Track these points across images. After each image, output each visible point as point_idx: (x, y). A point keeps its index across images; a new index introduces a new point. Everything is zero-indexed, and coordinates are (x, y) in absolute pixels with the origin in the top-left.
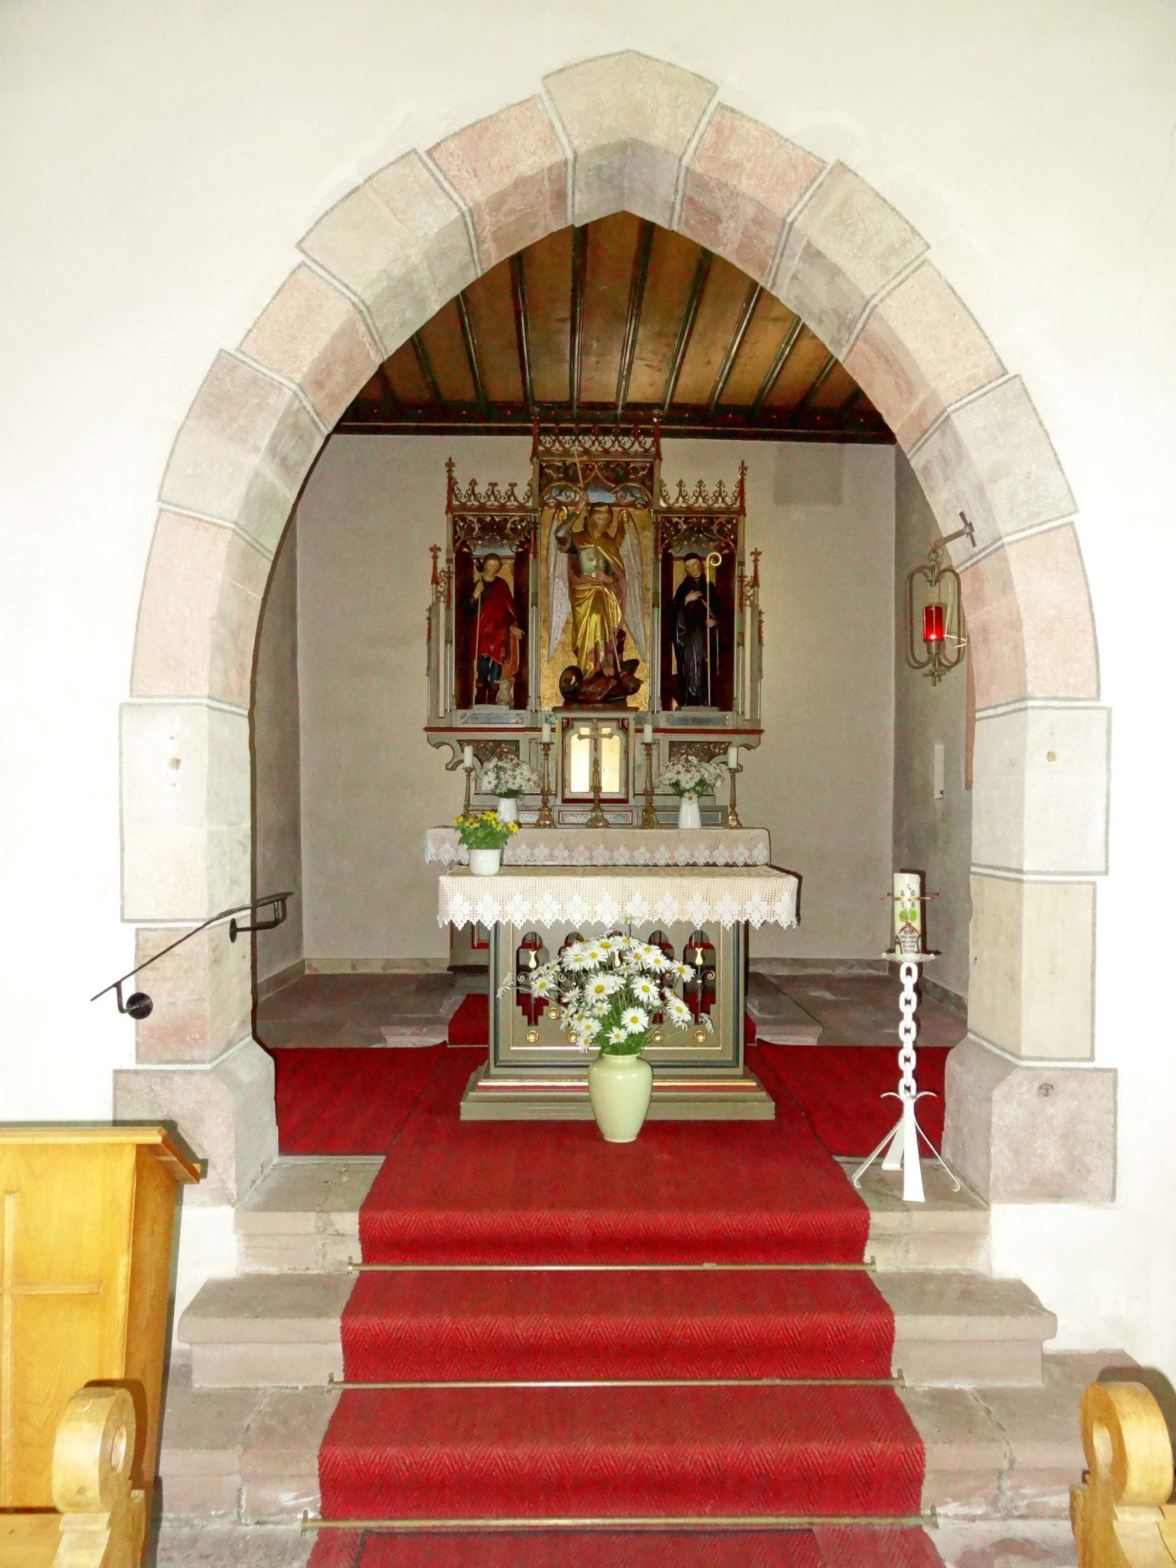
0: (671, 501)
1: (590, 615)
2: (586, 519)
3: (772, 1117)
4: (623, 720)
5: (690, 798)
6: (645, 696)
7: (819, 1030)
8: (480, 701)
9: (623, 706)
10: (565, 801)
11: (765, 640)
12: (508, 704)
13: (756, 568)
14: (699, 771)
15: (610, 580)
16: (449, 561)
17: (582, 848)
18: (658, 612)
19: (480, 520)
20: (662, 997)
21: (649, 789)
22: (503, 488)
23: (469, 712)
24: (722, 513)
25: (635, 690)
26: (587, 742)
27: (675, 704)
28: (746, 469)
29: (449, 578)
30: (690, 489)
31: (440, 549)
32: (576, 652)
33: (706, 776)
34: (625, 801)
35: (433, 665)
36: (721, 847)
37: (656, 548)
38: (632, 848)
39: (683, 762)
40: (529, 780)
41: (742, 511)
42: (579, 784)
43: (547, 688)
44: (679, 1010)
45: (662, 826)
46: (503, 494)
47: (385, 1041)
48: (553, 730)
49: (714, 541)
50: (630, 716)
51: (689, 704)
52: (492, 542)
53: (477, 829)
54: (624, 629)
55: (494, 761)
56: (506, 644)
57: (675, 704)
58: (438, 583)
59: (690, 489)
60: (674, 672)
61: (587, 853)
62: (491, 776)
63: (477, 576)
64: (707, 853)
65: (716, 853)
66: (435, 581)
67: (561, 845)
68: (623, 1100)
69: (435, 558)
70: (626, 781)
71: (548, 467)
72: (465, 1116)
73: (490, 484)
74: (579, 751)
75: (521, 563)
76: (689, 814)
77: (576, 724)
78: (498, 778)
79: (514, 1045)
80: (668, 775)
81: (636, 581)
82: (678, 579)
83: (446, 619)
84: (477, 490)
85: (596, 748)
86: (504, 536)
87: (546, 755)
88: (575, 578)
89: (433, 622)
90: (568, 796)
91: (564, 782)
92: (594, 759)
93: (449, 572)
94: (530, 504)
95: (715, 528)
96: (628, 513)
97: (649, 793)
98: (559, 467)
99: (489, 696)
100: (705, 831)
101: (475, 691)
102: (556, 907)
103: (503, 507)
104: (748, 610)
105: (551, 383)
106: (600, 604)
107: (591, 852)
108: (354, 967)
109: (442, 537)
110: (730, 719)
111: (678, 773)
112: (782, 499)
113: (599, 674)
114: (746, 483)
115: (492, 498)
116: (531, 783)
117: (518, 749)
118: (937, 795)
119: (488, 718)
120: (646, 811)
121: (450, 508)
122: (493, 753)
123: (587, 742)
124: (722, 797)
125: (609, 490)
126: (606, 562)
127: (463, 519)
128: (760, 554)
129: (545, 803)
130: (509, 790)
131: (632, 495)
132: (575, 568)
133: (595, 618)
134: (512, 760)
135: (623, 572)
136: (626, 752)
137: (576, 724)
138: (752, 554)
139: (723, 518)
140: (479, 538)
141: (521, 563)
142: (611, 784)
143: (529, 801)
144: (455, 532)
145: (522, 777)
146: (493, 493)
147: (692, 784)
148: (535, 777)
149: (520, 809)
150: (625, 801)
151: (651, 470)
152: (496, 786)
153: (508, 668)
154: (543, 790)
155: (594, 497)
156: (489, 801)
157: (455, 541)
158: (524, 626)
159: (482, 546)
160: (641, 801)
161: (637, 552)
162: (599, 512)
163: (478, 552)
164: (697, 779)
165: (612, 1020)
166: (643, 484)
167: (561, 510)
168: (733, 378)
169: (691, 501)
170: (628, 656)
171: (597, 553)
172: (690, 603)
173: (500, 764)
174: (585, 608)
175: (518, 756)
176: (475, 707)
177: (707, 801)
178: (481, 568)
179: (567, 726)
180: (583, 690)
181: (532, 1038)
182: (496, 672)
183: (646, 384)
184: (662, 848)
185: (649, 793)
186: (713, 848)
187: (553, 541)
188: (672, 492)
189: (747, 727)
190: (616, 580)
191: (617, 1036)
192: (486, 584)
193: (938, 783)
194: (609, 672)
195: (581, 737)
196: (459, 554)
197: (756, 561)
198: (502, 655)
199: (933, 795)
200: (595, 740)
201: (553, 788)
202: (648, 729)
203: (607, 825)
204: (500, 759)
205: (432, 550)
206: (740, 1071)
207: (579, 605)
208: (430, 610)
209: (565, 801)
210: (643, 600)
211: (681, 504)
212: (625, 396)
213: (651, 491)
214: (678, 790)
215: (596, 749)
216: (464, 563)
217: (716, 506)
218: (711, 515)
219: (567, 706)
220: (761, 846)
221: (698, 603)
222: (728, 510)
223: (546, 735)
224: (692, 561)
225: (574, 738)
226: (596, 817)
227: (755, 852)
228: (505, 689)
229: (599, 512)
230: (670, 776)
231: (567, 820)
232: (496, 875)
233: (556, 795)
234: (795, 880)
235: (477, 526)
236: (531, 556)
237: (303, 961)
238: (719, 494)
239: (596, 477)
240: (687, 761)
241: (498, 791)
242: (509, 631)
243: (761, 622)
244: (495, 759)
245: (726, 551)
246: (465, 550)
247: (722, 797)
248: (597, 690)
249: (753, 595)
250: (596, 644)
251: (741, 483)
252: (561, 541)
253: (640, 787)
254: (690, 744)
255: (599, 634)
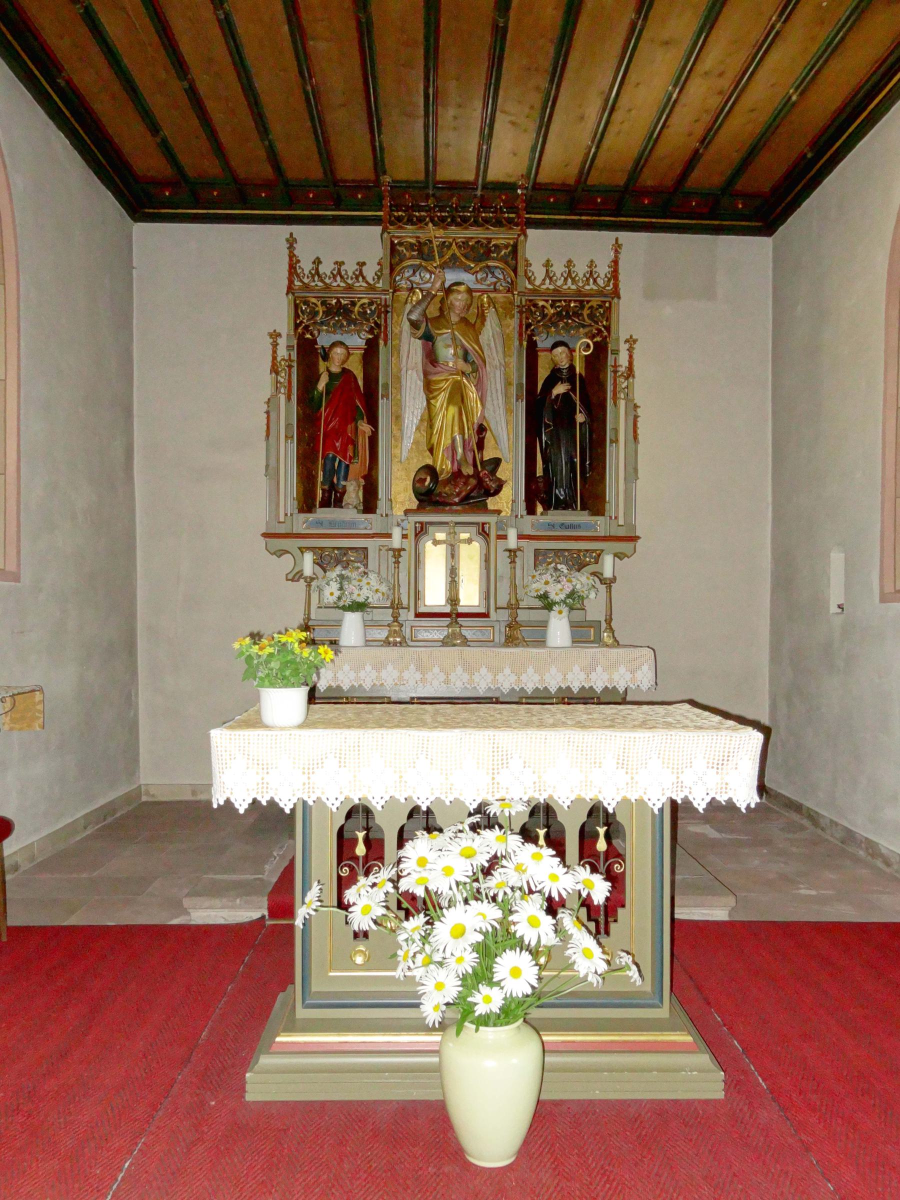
0: (537, 283)
1: (447, 409)
2: (442, 301)
3: (721, 1095)
4: (483, 524)
5: (560, 612)
6: (509, 498)
7: (731, 901)
8: (325, 504)
9: (483, 508)
10: (418, 615)
11: (640, 437)
12: (356, 507)
13: (631, 357)
14: (570, 581)
15: (468, 369)
16: (289, 348)
17: (436, 670)
18: (522, 406)
19: (323, 303)
20: (558, 929)
21: (513, 602)
22: (350, 268)
23: (311, 517)
24: (592, 296)
25: (497, 491)
26: (442, 548)
27: (540, 509)
28: (620, 246)
29: (290, 367)
30: (559, 269)
31: (280, 335)
32: (431, 450)
33: (578, 587)
34: (485, 615)
35: (273, 462)
36: (599, 669)
37: (520, 335)
38: (496, 670)
39: (551, 571)
40: (377, 591)
41: (616, 293)
42: (435, 596)
43: (398, 489)
44: (587, 954)
45: (526, 644)
46: (350, 274)
47: (189, 914)
48: (404, 536)
49: (584, 326)
50: (491, 519)
51: (556, 508)
52: (339, 326)
53: (271, 655)
54: (485, 424)
55: (338, 570)
56: (354, 443)
57: (540, 509)
58: (277, 373)
59: (559, 269)
60: (539, 472)
61: (442, 677)
62: (334, 586)
63: (322, 366)
64: (582, 676)
65: (593, 676)
66: (275, 370)
67: (412, 667)
68: (492, 1095)
69: (275, 345)
70: (486, 595)
71: (400, 244)
72: (251, 1096)
73: (336, 263)
74: (434, 558)
75: (370, 353)
76: (559, 628)
77: (431, 529)
78: (341, 589)
79: (331, 969)
80: (534, 586)
81: (498, 373)
82: (543, 374)
83: (287, 412)
84: (322, 270)
85: (453, 554)
86: (351, 322)
87: (398, 562)
88: (430, 368)
89: (273, 415)
90: (422, 610)
91: (418, 595)
92: (450, 568)
93: (290, 360)
94: (380, 285)
95: (586, 312)
96: (488, 297)
97: (513, 607)
98: (412, 245)
99: (333, 498)
100: (575, 651)
101: (319, 493)
102: (490, 677)
103: (349, 288)
104: (622, 404)
105: (405, 160)
106: (458, 396)
107: (448, 675)
108: (194, 793)
109: (284, 324)
110: (600, 526)
111: (547, 583)
112: (651, 293)
113: (457, 475)
114: (620, 263)
115: (338, 278)
116: (380, 594)
117: (366, 557)
118: (833, 609)
119: (332, 524)
120: (510, 626)
121: (290, 289)
122: (338, 562)
123: (442, 548)
124: (595, 610)
125: (468, 269)
126: (463, 347)
127: (306, 303)
128: (635, 341)
129: (396, 618)
130: (353, 602)
131: (494, 276)
132: (431, 357)
133: (453, 410)
134: (358, 568)
135: (484, 362)
136: (486, 560)
137: (431, 529)
138: (627, 341)
139: (595, 302)
140: (322, 323)
141: (370, 353)
142: (470, 596)
143: (378, 615)
144: (297, 316)
145: (369, 588)
146: (339, 273)
147: (562, 596)
148: (384, 588)
149: (367, 625)
150: (485, 615)
151: (515, 247)
152: (339, 598)
153: (358, 468)
154: (392, 603)
155: (451, 277)
156: (335, 614)
157: (297, 326)
158: (373, 421)
159: (327, 331)
160: (504, 616)
161: (497, 341)
162: (459, 292)
163: (324, 340)
164: (568, 591)
165: (483, 975)
166: (506, 263)
167: (414, 293)
168: (606, 143)
169: (559, 283)
170: (488, 455)
171: (454, 338)
172: (558, 395)
173: (343, 572)
174: (441, 400)
175: (366, 566)
176: (319, 510)
177: (578, 615)
178: (326, 358)
179: (421, 531)
180: (438, 491)
181: (359, 960)
182: (342, 473)
183: (508, 161)
184: (530, 670)
185: (513, 607)
186: (590, 669)
187: (406, 326)
188: (539, 274)
189: (622, 532)
190: (475, 370)
191: (488, 1000)
192: (331, 375)
193: (836, 595)
194: (468, 470)
195: (436, 543)
196: (301, 339)
197: (630, 350)
198: (350, 453)
199: (828, 609)
200: (452, 545)
201: (405, 602)
202: (512, 534)
203: (465, 642)
204: (345, 568)
205: (271, 335)
206: (663, 1012)
207: (434, 398)
208: (268, 402)
209: (418, 615)
210: (506, 396)
211: (547, 285)
212: (485, 176)
213: (515, 271)
214: (547, 603)
215: (453, 556)
216: (308, 353)
217: (587, 287)
218: (581, 298)
219: (420, 509)
220: (645, 668)
221: (566, 395)
222: (601, 293)
223: (396, 541)
224: (560, 349)
225: (429, 544)
226: (454, 633)
227: (639, 675)
228: (354, 492)
229: (459, 292)
230: (538, 586)
231: (420, 637)
232: (301, 726)
233: (408, 608)
234: (758, 737)
235: (320, 309)
236: (381, 342)
237: (140, 786)
238: (591, 275)
239: (454, 255)
240: (556, 569)
241: (341, 604)
242: (356, 428)
243: (636, 417)
244: (339, 568)
245: (598, 339)
246: (308, 336)
247: (595, 610)
248: (455, 491)
249: (627, 387)
250: (453, 440)
251: (616, 262)
252: (414, 325)
253: (503, 600)
254: (557, 552)
255: (456, 429)
